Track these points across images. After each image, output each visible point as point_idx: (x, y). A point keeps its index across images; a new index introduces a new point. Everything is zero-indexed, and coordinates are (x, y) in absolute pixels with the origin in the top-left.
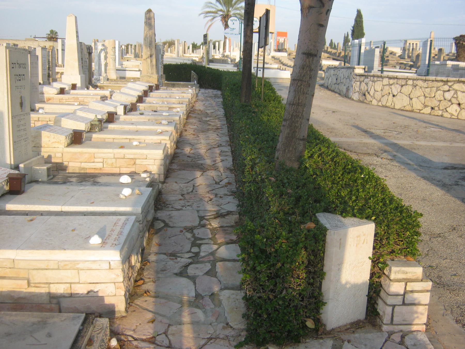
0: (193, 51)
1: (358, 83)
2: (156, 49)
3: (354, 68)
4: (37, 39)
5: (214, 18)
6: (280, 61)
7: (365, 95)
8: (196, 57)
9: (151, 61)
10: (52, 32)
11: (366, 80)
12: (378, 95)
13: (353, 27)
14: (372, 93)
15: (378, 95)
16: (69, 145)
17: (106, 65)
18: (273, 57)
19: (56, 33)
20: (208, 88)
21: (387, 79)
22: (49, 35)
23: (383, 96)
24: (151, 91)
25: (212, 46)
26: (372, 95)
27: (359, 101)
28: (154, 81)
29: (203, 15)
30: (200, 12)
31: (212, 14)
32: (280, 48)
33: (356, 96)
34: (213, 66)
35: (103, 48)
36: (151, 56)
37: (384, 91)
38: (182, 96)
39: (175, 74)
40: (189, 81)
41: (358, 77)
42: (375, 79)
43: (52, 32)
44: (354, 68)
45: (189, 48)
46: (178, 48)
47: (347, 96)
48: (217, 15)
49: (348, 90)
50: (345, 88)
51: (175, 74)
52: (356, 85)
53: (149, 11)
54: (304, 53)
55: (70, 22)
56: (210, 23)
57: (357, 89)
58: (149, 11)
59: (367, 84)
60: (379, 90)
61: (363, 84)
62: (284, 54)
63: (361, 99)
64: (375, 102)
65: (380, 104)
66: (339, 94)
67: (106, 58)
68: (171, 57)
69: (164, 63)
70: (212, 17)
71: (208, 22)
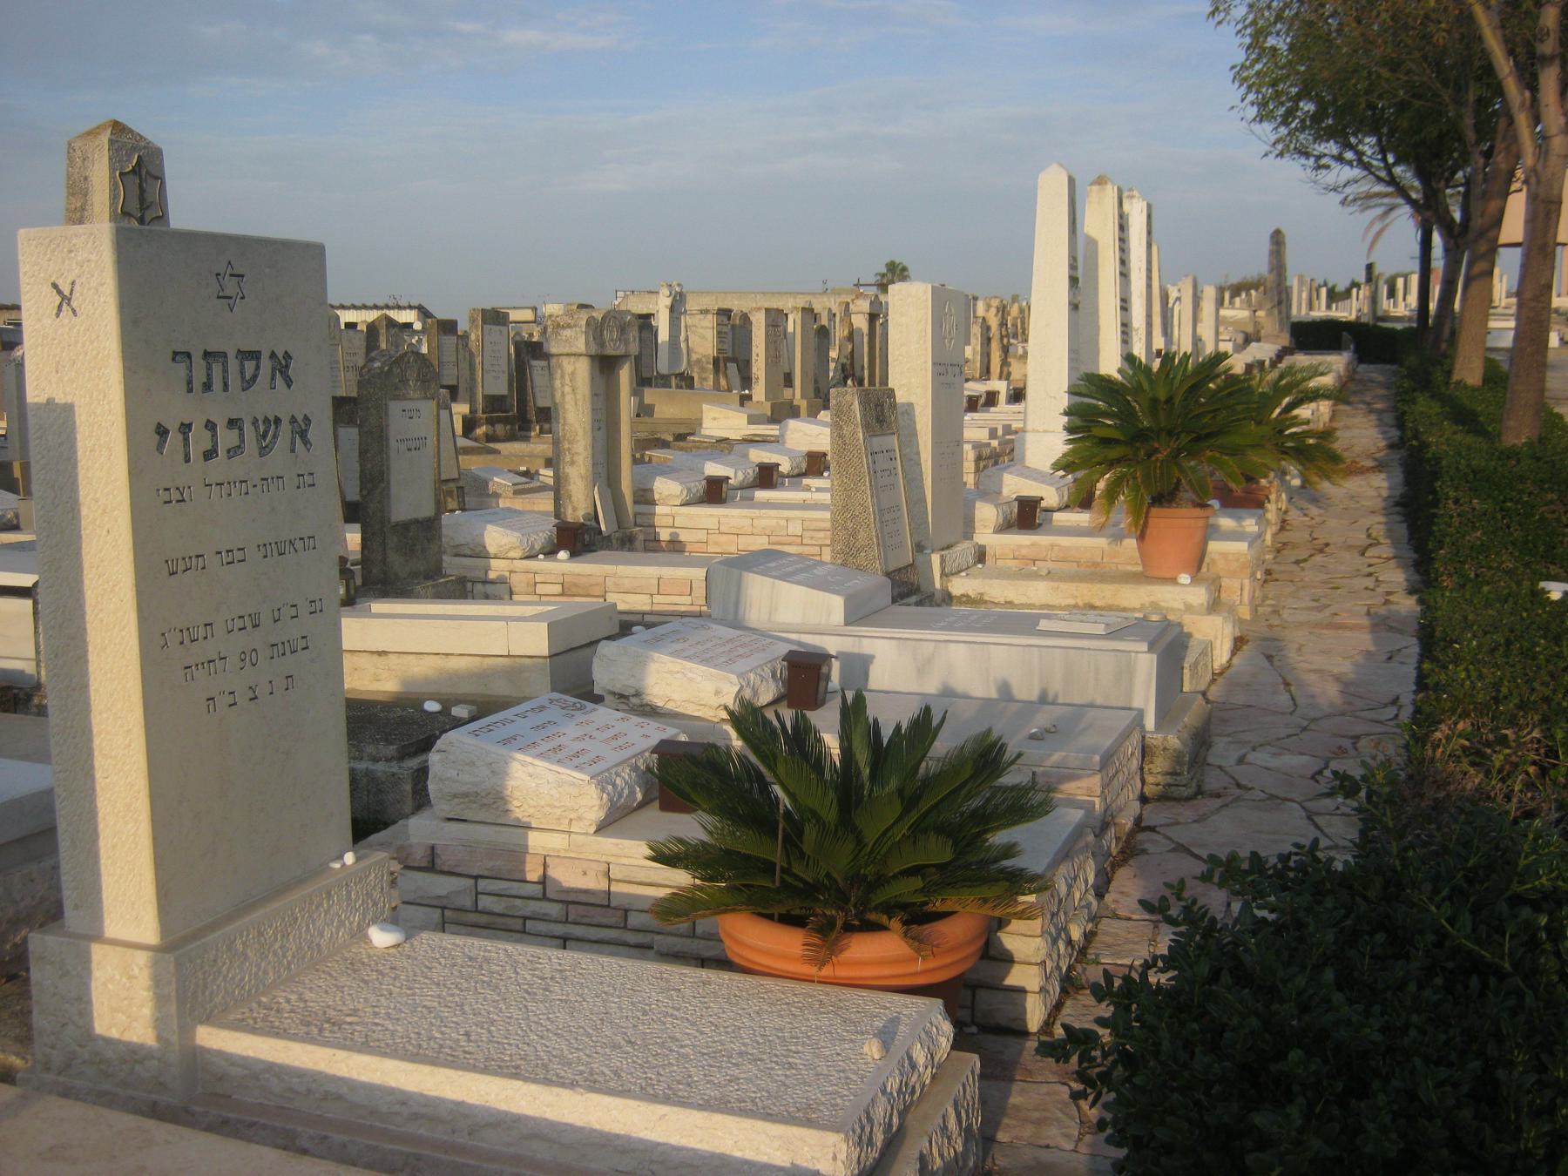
0: (1329, 307)
8: (1346, 312)
22: (883, 275)
25: (1384, 290)
36: (1280, 303)
56: (1378, 226)
68: (1300, 310)
71: (1372, 223)
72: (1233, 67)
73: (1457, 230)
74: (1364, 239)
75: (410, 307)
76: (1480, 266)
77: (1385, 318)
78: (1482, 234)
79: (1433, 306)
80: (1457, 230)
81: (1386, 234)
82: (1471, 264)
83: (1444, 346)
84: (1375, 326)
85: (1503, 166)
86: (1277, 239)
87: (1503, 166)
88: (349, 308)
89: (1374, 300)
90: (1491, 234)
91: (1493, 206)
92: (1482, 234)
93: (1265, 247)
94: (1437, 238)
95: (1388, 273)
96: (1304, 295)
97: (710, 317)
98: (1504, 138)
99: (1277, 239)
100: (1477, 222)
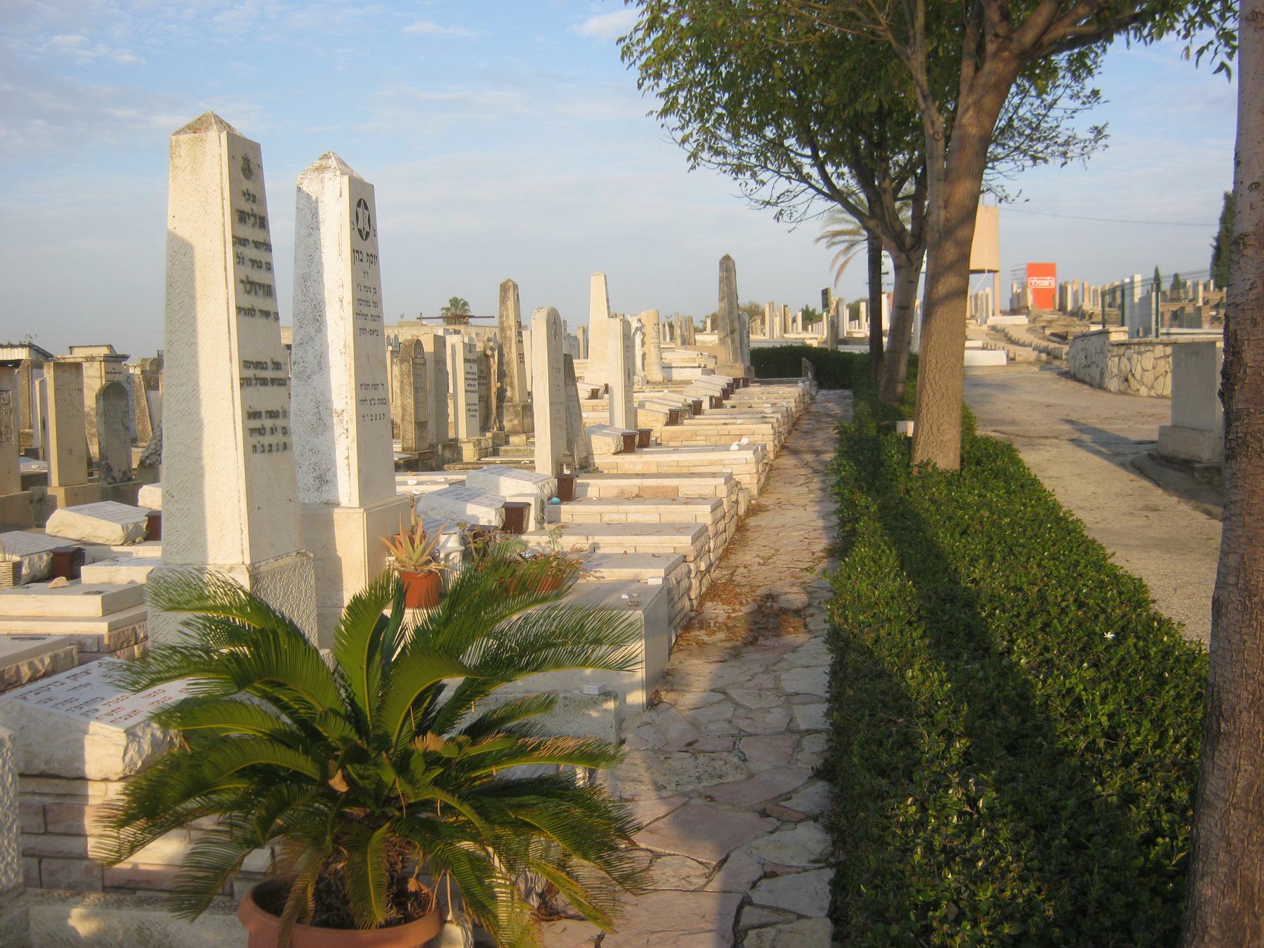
0: (805, 328)
1: (1116, 359)
2: (735, 318)
3: (1108, 332)
4: (424, 322)
5: (852, 245)
6: (1006, 335)
7: (1127, 380)
8: (815, 337)
9: (733, 341)
10: (455, 302)
11: (1129, 352)
12: (1148, 378)
13: (1218, 239)
14: (1138, 374)
15: (1148, 378)
16: (667, 424)
17: (644, 356)
18: (993, 328)
19: (465, 304)
20: (834, 388)
21: (1160, 347)
22: (448, 309)
23: (1156, 379)
24: (738, 387)
25: (846, 314)
26: (1138, 377)
27: (1121, 393)
28: (739, 372)
29: (824, 241)
30: (819, 235)
31: (847, 238)
32: (1015, 307)
33: (1113, 384)
34: (843, 349)
35: (639, 325)
36: (732, 332)
37: (1158, 368)
38: (788, 394)
39: (772, 364)
40: (799, 375)
41: (1115, 349)
42: (1142, 348)
43: (455, 302)
44: (1108, 332)
45: (794, 320)
46: (772, 321)
47: (1101, 387)
48: (857, 238)
49: (1102, 374)
50: (1098, 370)
51: (772, 364)
52: (1113, 364)
53: (727, 259)
54: (242, 282)
55: (597, 284)
56: (842, 260)
57: (1115, 371)
58: (727, 259)
59: (1129, 359)
60: (1150, 367)
61: (1124, 360)
62: (1022, 320)
63: (1122, 389)
64: (1144, 391)
65: (1153, 393)
66: (1091, 385)
67: (643, 343)
68: (762, 337)
69: (753, 345)
70: (843, 246)
71: (837, 257)
72: (621, 40)
73: (908, 241)
74: (831, 269)
75: (22, 346)
76: (948, 283)
77: (845, 342)
78: (948, 232)
79: (886, 325)
80: (908, 241)
81: (848, 267)
82: (932, 280)
83: (900, 388)
84: (835, 352)
85: (973, 131)
86: (727, 265)
87: (973, 131)
88: (16, 347)
89: (834, 326)
90: (961, 234)
91: (961, 191)
92: (948, 232)
93: (715, 273)
94: (888, 263)
95: (851, 300)
96: (777, 320)
97: (97, 364)
98: (972, 88)
99: (727, 265)
100: (939, 217)
